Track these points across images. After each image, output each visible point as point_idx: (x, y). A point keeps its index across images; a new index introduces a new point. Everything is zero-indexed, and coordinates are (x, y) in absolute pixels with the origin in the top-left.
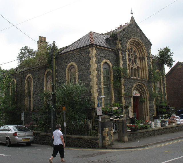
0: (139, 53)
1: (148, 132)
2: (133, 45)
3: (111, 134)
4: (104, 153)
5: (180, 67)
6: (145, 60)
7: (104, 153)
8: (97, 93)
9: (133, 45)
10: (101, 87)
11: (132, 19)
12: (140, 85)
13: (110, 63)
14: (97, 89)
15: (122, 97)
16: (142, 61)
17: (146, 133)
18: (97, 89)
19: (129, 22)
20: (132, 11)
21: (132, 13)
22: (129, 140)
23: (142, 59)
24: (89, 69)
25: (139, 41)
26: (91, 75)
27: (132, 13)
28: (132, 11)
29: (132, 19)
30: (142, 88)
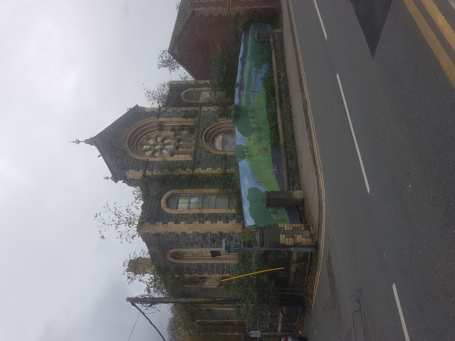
0: (151, 131)
1: (286, 143)
2: (137, 144)
3: (291, 229)
4: (329, 261)
5: (176, 52)
6: (163, 122)
7: (329, 261)
8: (218, 222)
9: (137, 144)
10: (207, 214)
11: (91, 141)
12: (205, 139)
13: (168, 194)
14: (212, 223)
15: (225, 174)
16: (166, 126)
17: (289, 147)
18: (212, 223)
19: (94, 148)
20: (74, 142)
21: (78, 142)
22: (300, 189)
23: (161, 127)
24: (177, 235)
25: (131, 133)
26: (187, 232)
27: (78, 142)
28: (74, 142)
29: (91, 141)
30: (211, 131)
